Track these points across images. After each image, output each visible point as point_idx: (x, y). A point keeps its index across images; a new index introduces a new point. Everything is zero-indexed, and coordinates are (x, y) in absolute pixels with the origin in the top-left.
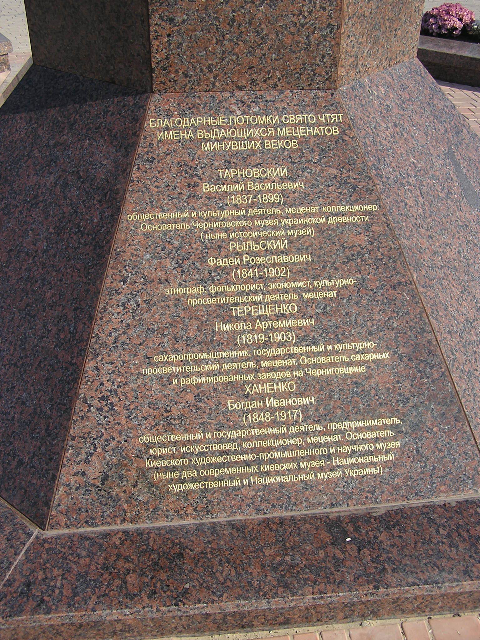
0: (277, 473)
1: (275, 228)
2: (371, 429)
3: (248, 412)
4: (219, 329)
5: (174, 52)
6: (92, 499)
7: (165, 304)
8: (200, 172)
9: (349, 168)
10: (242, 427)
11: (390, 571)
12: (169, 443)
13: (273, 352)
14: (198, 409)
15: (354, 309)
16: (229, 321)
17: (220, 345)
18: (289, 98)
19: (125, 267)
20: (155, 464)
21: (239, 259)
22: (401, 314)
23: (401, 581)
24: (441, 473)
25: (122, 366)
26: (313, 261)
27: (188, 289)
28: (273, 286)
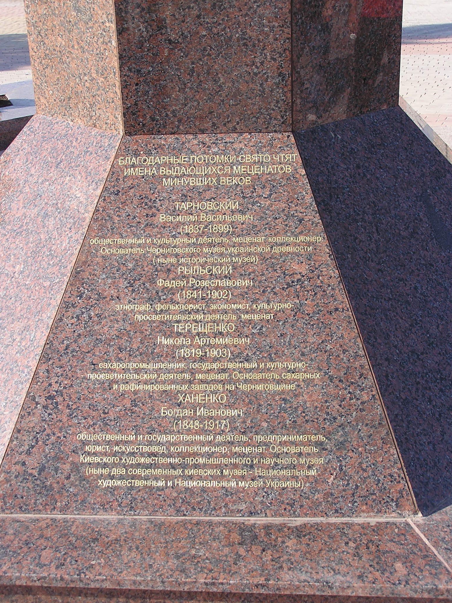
0: (200, 478)
1: (221, 255)
2: (295, 444)
3: (178, 419)
4: (161, 342)
5: (142, 99)
6: (28, 487)
7: (114, 318)
8: (158, 204)
9: (298, 203)
10: (171, 432)
11: (286, 569)
12: (104, 441)
13: (208, 366)
14: (133, 413)
15: (289, 331)
16: (170, 336)
17: (159, 357)
18: (247, 140)
19: (83, 284)
20: (88, 459)
21: (185, 281)
22: (335, 338)
23: (294, 577)
24: (363, 493)
25: (69, 370)
26: (254, 286)
27: (136, 305)
28: (214, 307)
